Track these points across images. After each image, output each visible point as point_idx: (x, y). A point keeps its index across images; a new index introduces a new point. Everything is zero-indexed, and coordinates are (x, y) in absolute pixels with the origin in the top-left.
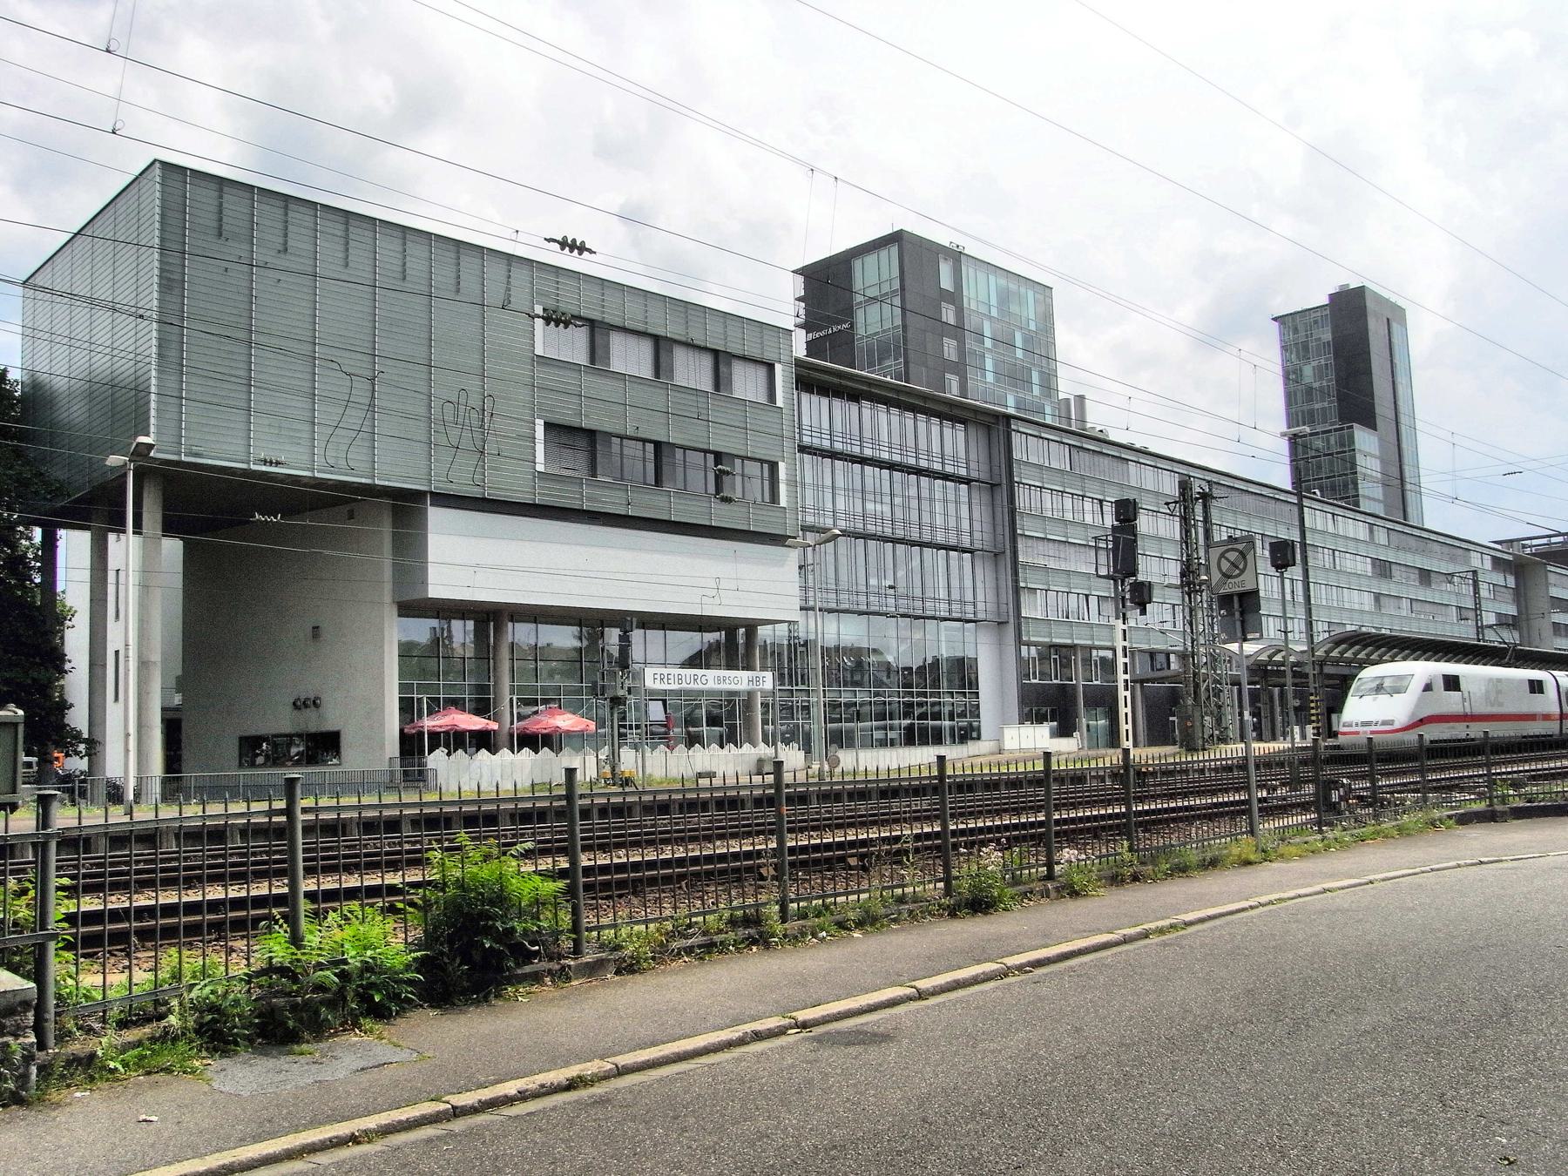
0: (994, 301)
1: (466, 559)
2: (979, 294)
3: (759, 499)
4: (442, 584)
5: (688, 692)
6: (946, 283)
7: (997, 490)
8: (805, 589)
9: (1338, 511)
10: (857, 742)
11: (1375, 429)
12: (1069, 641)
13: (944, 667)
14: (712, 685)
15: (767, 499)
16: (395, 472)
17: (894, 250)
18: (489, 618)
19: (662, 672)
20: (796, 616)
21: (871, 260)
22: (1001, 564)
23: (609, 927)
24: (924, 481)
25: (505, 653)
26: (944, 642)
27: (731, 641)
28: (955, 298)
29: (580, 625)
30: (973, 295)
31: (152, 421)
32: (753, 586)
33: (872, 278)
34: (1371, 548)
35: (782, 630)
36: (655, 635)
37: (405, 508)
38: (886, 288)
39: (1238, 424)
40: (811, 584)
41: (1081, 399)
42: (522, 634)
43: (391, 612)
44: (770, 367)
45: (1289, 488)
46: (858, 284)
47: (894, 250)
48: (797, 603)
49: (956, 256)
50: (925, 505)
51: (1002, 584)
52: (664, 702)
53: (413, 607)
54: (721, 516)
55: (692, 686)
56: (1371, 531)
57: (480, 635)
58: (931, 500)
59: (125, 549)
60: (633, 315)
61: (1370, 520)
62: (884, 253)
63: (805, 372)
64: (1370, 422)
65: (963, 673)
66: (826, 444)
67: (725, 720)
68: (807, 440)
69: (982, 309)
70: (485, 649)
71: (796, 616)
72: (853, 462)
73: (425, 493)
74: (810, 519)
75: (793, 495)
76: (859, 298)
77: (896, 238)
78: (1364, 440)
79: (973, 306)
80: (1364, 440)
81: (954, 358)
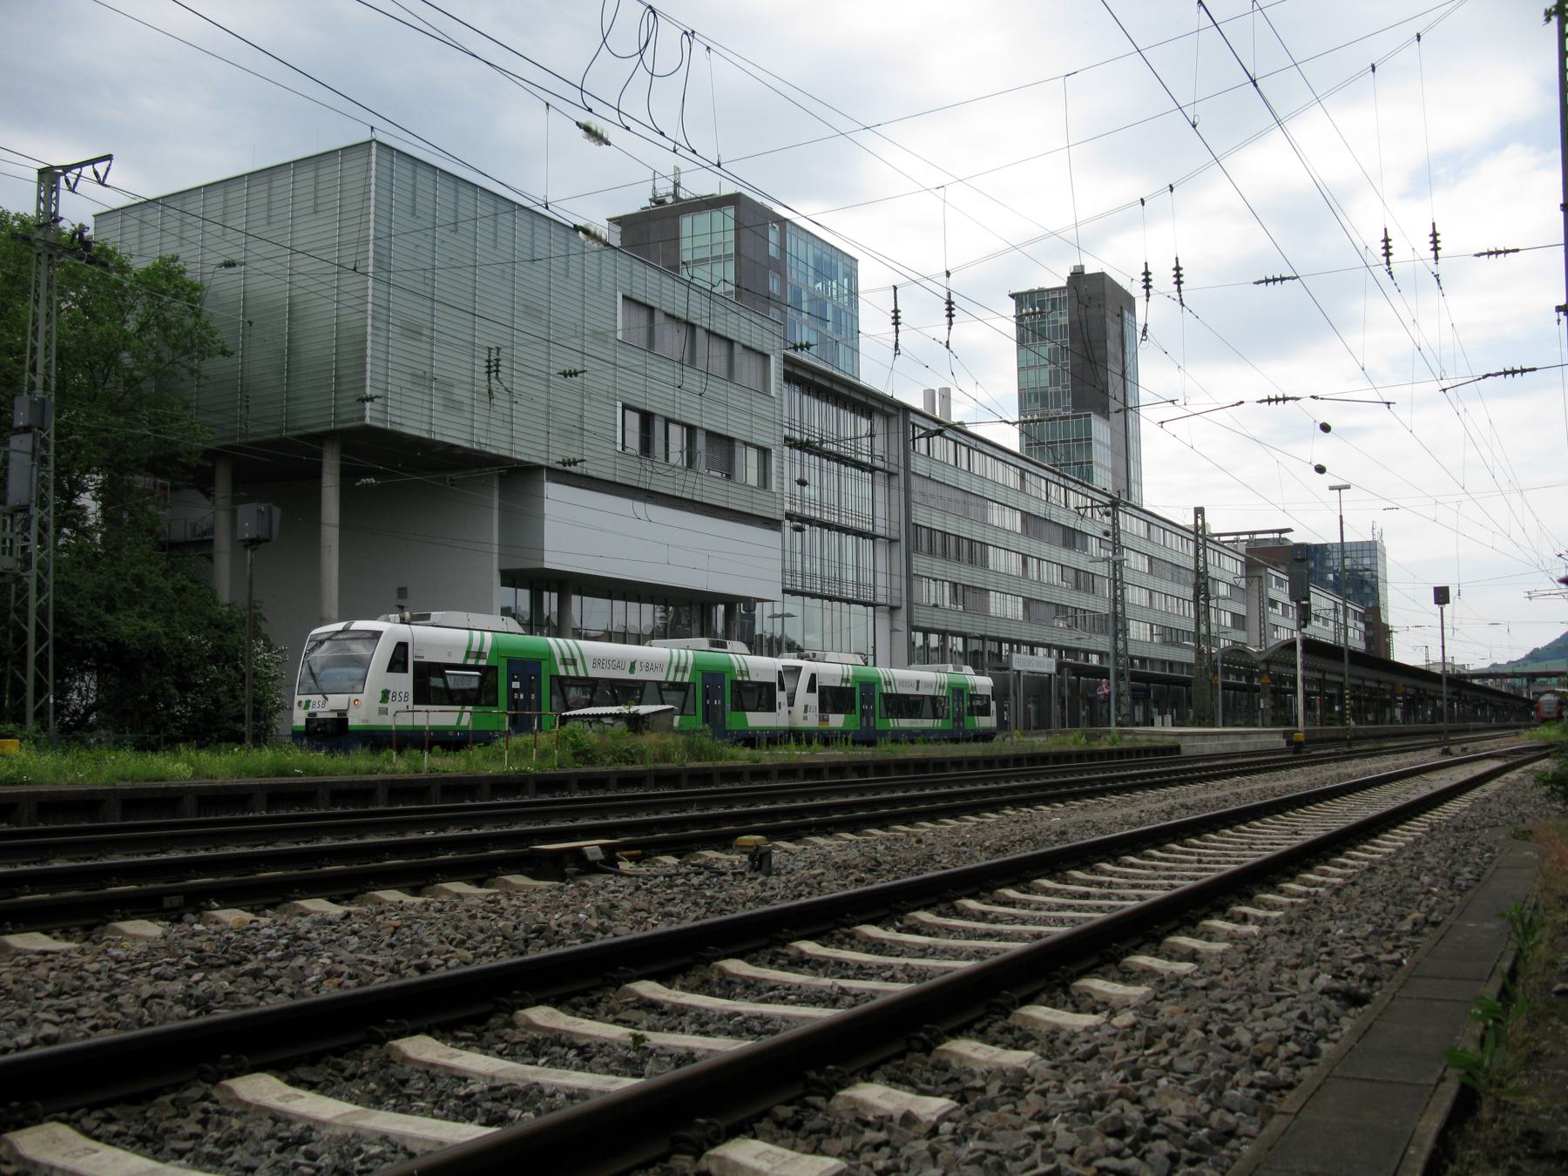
7: (894, 482)
9: (1071, 485)
10: (765, 650)
11: (1108, 418)
16: (527, 450)
17: (731, 211)
21: (702, 220)
23: (926, 638)
28: (779, 266)
34: (1022, 497)
37: (517, 479)
38: (718, 251)
39: (986, 387)
45: (1016, 449)
47: (731, 211)
54: (710, 488)
56: (1023, 478)
61: (1149, 518)
62: (718, 215)
63: (790, 369)
64: (1104, 413)
71: (778, 595)
77: (735, 200)
78: (1100, 430)
80: (1100, 430)
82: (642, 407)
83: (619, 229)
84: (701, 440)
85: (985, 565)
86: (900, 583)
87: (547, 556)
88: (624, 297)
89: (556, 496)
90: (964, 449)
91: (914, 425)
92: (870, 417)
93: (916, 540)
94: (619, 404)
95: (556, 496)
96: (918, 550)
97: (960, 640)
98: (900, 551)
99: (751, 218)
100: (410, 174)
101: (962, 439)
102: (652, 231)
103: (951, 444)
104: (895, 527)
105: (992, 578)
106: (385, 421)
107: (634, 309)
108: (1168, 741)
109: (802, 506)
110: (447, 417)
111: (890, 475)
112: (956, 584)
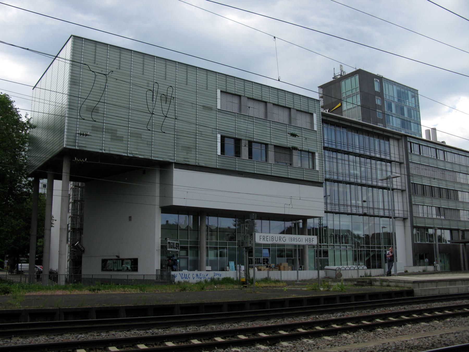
0: (396, 95)
1: (190, 189)
2: (390, 93)
3: (308, 167)
4: (178, 200)
5: (279, 245)
6: (377, 89)
7: (402, 165)
8: (326, 203)
12: (457, 228)
13: (382, 236)
14: (288, 242)
15: (311, 167)
17: (357, 77)
18: (199, 214)
19: (267, 236)
20: (322, 214)
21: (348, 81)
22: (405, 195)
24: (373, 162)
25: (204, 228)
26: (381, 226)
27: (296, 223)
28: (381, 94)
29: (235, 218)
30: (387, 93)
31: (65, 133)
32: (307, 201)
33: (349, 88)
35: (317, 221)
36: (266, 223)
37: (164, 167)
38: (354, 91)
40: (328, 201)
41: (434, 130)
42: (212, 221)
43: (158, 211)
44: (312, 114)
46: (343, 90)
47: (357, 77)
48: (323, 209)
49: (381, 78)
50: (374, 171)
51: (405, 201)
52: (269, 249)
53: (168, 209)
55: (279, 242)
57: (195, 221)
58: (376, 169)
59: (58, 184)
60: (256, 94)
62: (353, 79)
63: (325, 118)
65: (389, 239)
66: (334, 147)
67: (294, 257)
68: (326, 145)
69: (391, 99)
70: (196, 228)
71: (322, 214)
72: (345, 154)
73: (172, 163)
74: (328, 176)
75: (321, 164)
76: (344, 95)
77: (359, 72)
79: (388, 98)
81: (381, 117)
82: (234, 136)
83: (321, 90)
84: (271, 149)
85: (456, 199)
86: (407, 207)
87: (174, 200)
88: (221, 91)
89: (178, 175)
90: (441, 152)
91: (411, 143)
92: (389, 141)
93: (414, 190)
94: (219, 136)
95: (178, 175)
96: (416, 193)
97: (448, 232)
98: (406, 194)
99: (364, 77)
100: (94, 48)
101: (446, 149)
102: (331, 90)
103: (434, 150)
104: (404, 185)
105: (461, 205)
106: (102, 150)
107: (230, 98)
108: (407, 287)
109: (338, 176)
110: (113, 144)
111: (401, 163)
112: (439, 208)
